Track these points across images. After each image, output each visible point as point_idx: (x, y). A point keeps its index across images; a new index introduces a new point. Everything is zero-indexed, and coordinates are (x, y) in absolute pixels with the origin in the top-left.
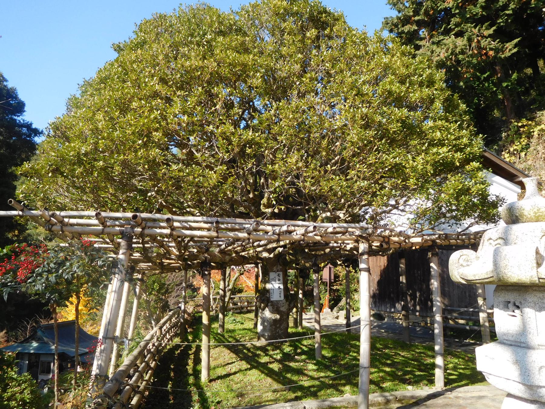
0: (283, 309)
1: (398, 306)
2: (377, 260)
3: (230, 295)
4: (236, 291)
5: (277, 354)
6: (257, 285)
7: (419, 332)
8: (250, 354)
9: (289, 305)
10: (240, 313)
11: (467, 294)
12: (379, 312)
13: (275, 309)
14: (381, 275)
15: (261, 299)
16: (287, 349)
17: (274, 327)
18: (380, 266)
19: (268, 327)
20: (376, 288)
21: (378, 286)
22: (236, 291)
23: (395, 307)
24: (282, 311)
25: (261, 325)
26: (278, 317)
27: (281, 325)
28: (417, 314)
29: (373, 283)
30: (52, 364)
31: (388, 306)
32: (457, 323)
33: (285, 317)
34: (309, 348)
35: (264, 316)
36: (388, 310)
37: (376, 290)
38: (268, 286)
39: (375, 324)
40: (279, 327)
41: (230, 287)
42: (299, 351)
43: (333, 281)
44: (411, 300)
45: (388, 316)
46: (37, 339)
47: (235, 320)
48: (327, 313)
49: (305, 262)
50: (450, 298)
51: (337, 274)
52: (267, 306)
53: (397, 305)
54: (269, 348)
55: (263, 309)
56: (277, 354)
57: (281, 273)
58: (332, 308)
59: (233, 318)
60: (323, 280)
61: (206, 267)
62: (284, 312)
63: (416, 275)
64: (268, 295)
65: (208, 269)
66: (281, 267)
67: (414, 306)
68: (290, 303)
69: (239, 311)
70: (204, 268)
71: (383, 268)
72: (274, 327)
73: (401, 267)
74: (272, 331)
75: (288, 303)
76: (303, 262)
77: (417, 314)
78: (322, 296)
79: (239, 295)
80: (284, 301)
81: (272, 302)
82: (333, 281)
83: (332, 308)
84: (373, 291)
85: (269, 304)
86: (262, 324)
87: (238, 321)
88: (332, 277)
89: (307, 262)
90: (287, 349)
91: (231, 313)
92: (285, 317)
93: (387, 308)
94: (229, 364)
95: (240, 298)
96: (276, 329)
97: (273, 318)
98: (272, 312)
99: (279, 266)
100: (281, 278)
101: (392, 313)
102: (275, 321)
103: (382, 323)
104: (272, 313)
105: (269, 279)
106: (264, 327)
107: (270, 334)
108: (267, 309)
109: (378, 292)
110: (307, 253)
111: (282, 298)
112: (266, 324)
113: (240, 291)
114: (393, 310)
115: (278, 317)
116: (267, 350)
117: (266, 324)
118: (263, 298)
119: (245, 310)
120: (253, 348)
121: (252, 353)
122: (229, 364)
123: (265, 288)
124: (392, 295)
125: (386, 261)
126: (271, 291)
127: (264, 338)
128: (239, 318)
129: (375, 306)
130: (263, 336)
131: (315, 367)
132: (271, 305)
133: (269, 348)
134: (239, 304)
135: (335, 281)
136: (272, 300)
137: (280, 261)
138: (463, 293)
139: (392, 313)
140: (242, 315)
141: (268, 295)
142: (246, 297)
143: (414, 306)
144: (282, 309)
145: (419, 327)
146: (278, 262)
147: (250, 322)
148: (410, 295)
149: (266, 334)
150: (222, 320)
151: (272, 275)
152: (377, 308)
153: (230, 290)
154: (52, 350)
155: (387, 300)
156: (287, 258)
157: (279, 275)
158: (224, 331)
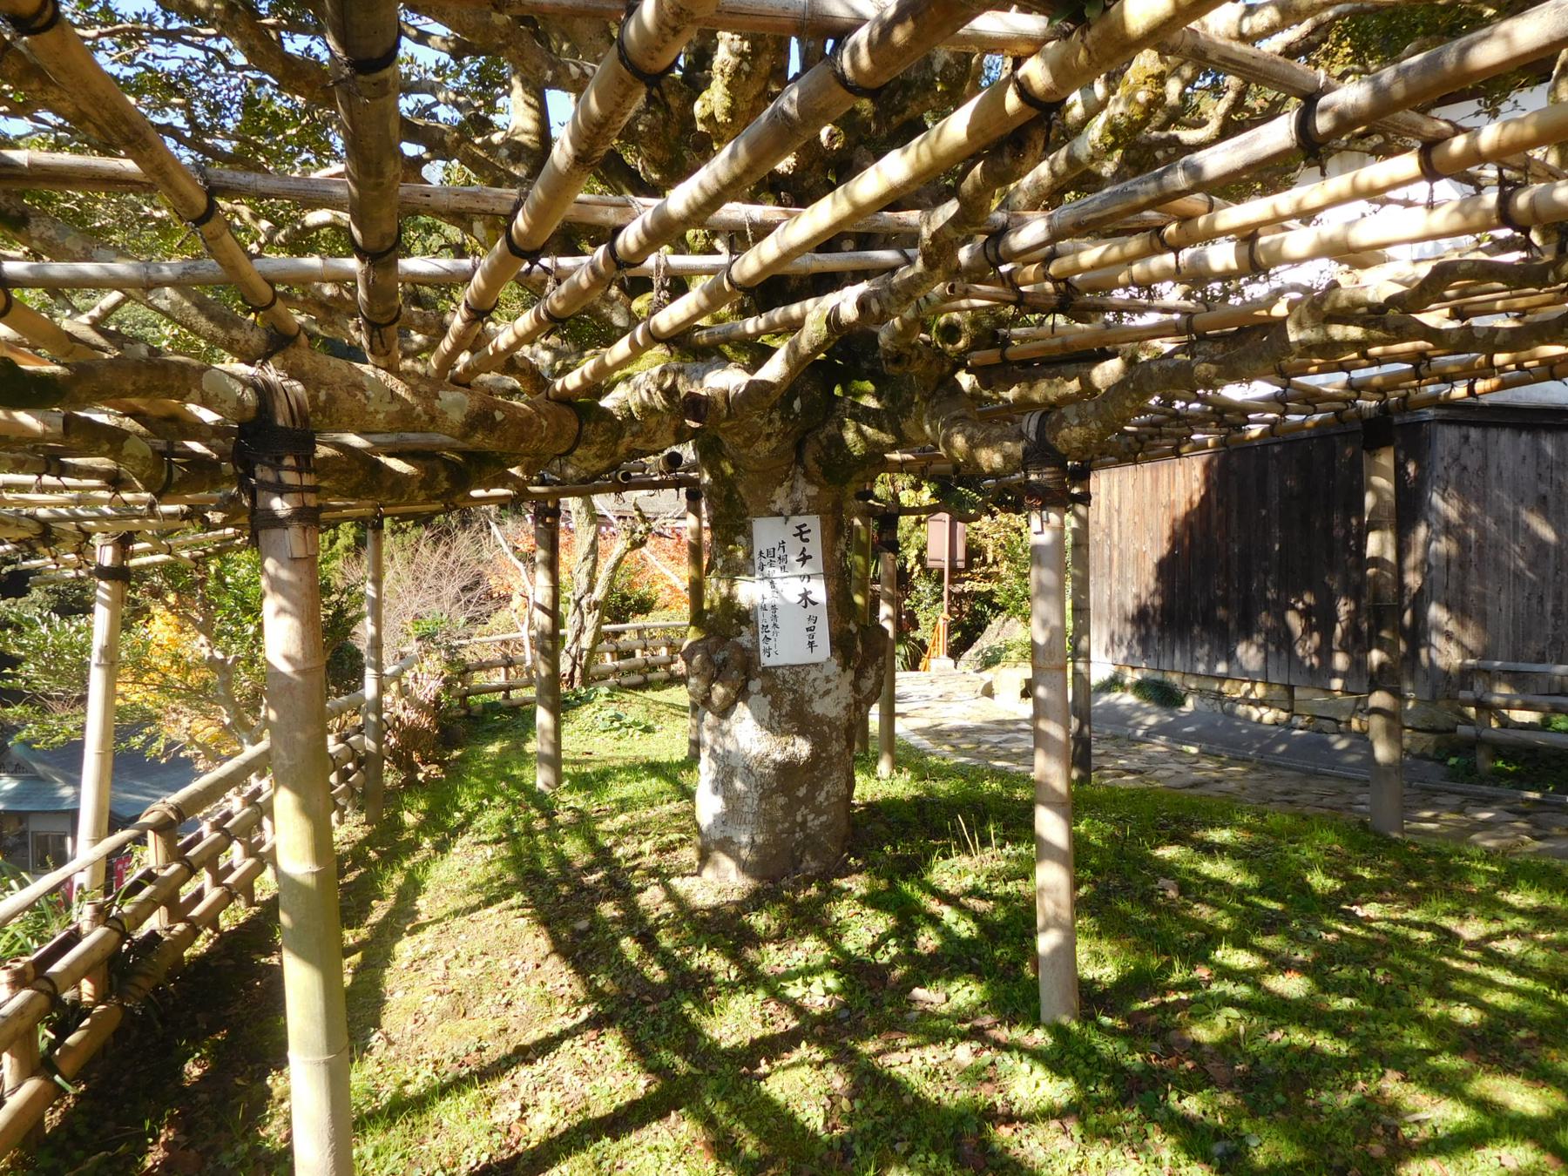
0: (829, 707)
1: (1249, 654)
2: (1156, 481)
3: (600, 622)
4: (623, 606)
5: (811, 971)
6: (696, 589)
7: (1351, 758)
8: (656, 973)
9: (856, 687)
10: (644, 685)
11: (1549, 607)
12: (1158, 676)
13: (788, 705)
14: (1175, 539)
15: (708, 659)
16: (863, 929)
17: (782, 800)
18: (1171, 505)
19: (752, 803)
20: (1152, 585)
21: (1157, 580)
22: (623, 606)
23: (1230, 657)
24: (820, 720)
25: (715, 790)
26: (802, 748)
27: (815, 787)
28: (1337, 684)
29: (1139, 570)
30: (69, 840)
31: (1202, 652)
32: (1506, 723)
33: (836, 748)
34: (976, 917)
35: (729, 744)
36: (1201, 668)
37: (1153, 594)
38: (748, 592)
39: (1151, 720)
40: (811, 797)
41: (599, 594)
42: (928, 940)
43: (961, 565)
44: (1308, 630)
45: (1200, 691)
46: (11, 769)
47: (619, 718)
48: (943, 675)
49: (973, 445)
50: (1483, 620)
51: (973, 541)
52: (742, 694)
53: (1241, 649)
54: (759, 921)
55: (724, 713)
56: (811, 971)
57: (813, 523)
58: (955, 652)
59: (611, 711)
60: (930, 564)
61: (277, 466)
62: (831, 723)
63: (1339, 532)
64: (745, 640)
65: (290, 478)
66: (812, 491)
67: (1325, 652)
68: (860, 674)
69: (637, 678)
70: (263, 473)
71: (1181, 509)
72: (782, 800)
73: (1378, 492)
74: (772, 823)
75: (850, 675)
76: (959, 441)
77: (1337, 684)
78: (920, 617)
79: (638, 621)
80: (834, 667)
81: (768, 672)
82: (961, 565)
83: (955, 652)
84: (1138, 596)
85: (755, 685)
86: (722, 784)
87: (628, 720)
88: (961, 554)
89: (988, 442)
90: (863, 929)
91: (604, 690)
92: (836, 748)
93: (1195, 660)
94: (525, 1054)
95: (640, 631)
96: (789, 810)
97: (779, 757)
98: (773, 725)
99: (801, 483)
100: (815, 547)
101: (1222, 679)
102: (787, 771)
103: (1178, 718)
104: (771, 729)
105: (749, 555)
106: (731, 798)
107: (759, 839)
108: (742, 711)
109: (1157, 601)
110: (974, 396)
111: (823, 651)
112: (739, 785)
113: (644, 606)
114: (1221, 668)
115: (802, 748)
116: (752, 938)
117: (739, 785)
118: (719, 657)
119: (661, 673)
120: (676, 927)
121: (666, 960)
122: (525, 1054)
123: (729, 601)
124: (1221, 613)
125: (1196, 485)
126: (764, 618)
127: (735, 857)
128: (635, 707)
129: (1145, 655)
130: (727, 845)
131: (1058, 1091)
132: (764, 691)
133: (759, 921)
134: (638, 653)
135: (969, 564)
136: (766, 661)
137: (809, 459)
138: (1534, 601)
139: (1222, 679)
140: (650, 694)
141: (745, 640)
142: (665, 629)
143: (1325, 652)
144: (820, 707)
145: (1342, 734)
146: (799, 460)
147: (679, 721)
148: (1305, 614)
149: (745, 839)
150: (551, 737)
151: (766, 532)
152: (1153, 660)
153: (596, 605)
154: (63, 799)
155: (1196, 630)
156: (850, 436)
157: (801, 532)
158: (559, 782)
